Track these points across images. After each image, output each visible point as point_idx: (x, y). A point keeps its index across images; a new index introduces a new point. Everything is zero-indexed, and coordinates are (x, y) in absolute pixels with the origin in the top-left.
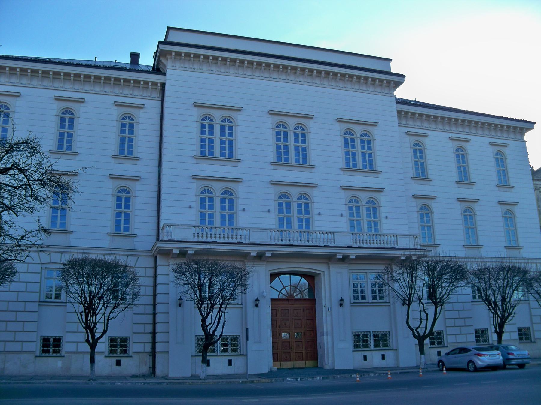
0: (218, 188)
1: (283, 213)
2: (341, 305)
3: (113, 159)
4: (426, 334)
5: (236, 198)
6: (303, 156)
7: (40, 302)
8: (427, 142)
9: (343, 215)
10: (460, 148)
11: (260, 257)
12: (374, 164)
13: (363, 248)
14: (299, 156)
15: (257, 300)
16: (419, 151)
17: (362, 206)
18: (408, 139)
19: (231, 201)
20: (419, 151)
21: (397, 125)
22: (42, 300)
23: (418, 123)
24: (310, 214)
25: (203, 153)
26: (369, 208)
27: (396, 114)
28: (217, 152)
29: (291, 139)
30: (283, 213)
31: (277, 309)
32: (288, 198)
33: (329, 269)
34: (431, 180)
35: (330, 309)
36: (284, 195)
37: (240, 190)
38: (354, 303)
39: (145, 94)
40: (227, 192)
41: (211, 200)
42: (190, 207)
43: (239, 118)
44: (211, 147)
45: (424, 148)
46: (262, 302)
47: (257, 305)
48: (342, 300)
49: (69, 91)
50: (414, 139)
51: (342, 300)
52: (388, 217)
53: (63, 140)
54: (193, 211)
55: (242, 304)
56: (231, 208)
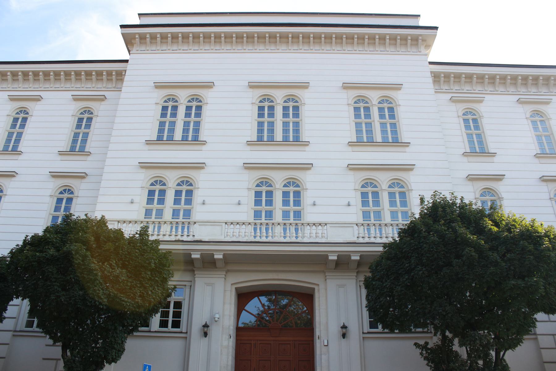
0: (278, 179)
2: (344, 336)
5: (409, 190)
7: (15, 331)
10: (537, 113)
12: (483, 139)
15: (206, 326)
16: (472, 122)
19: (297, 194)
20: (472, 122)
21: (433, 91)
22: (18, 329)
23: (467, 88)
25: (260, 139)
27: (430, 80)
28: (279, 135)
29: (278, 117)
32: (375, 186)
33: (326, 280)
35: (326, 344)
36: (264, 182)
37: (308, 179)
38: (368, 333)
41: (270, 194)
42: (349, 205)
43: (306, 97)
44: (271, 131)
45: (480, 117)
46: (214, 331)
47: (206, 334)
48: (344, 327)
50: (462, 107)
52: (206, 202)
54: (352, 209)
55: (187, 333)
56: (297, 203)
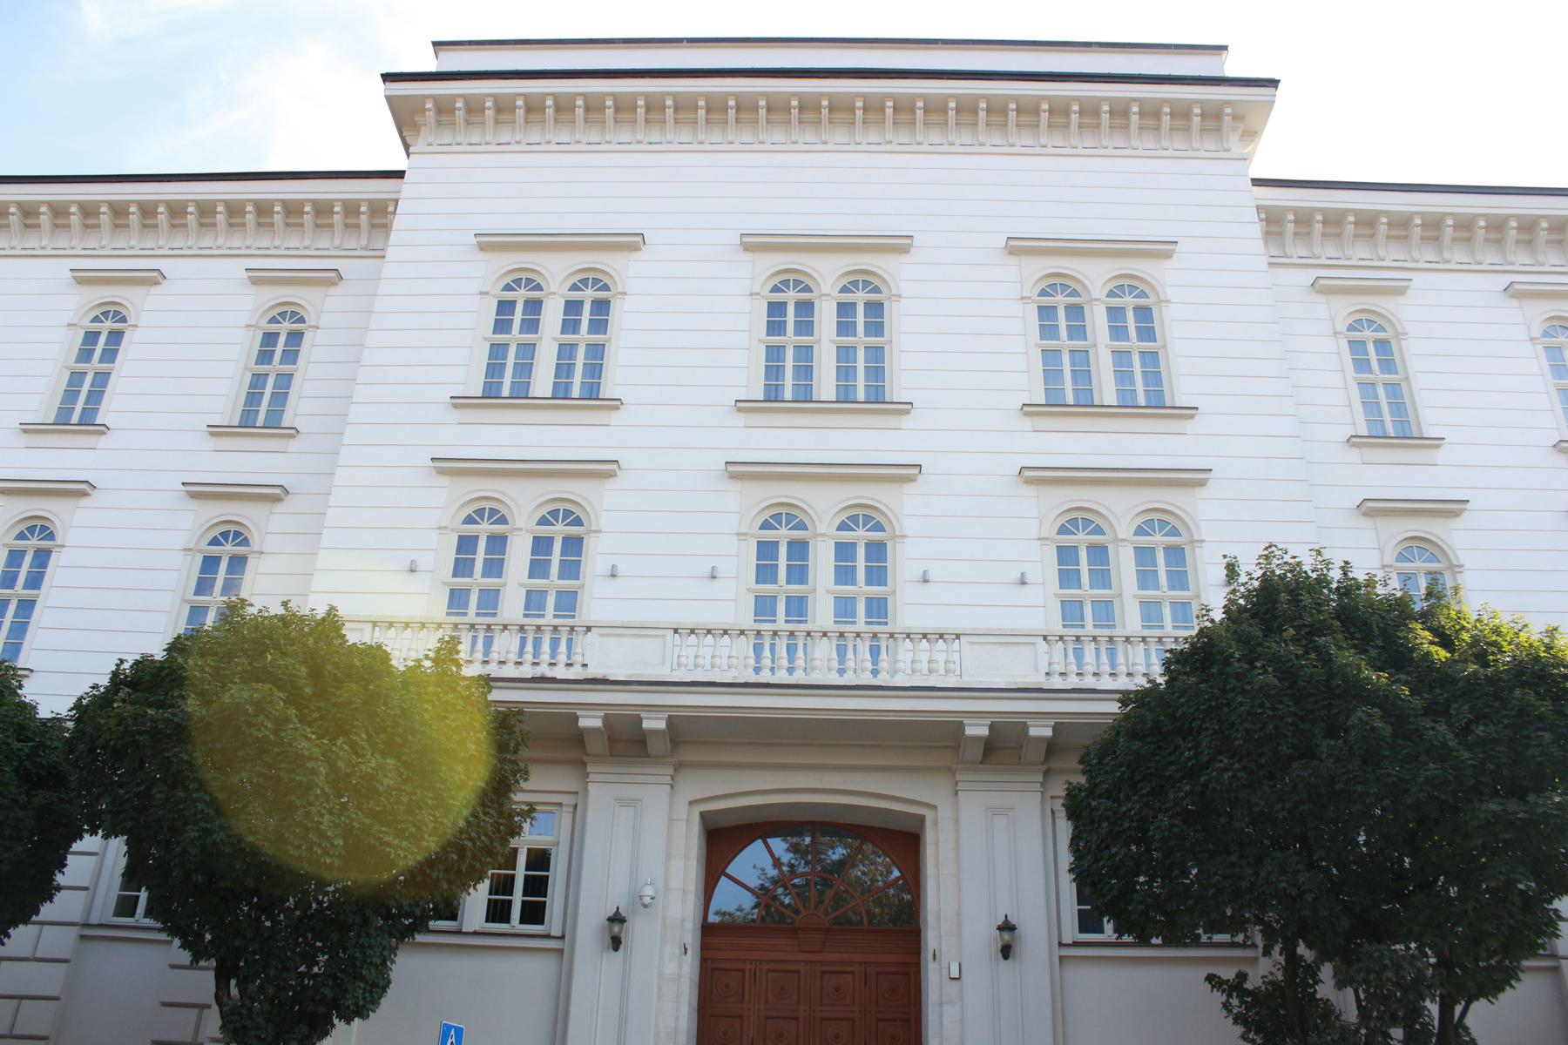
0: (824, 507)
1: (1157, 588)
3: (742, 416)
4: (159, 925)
6: (1146, 383)
8: (1402, 311)
9: (1029, 578)
11: (626, 743)
13: (553, 680)
14: (74, 401)
15: (617, 919)
17: (1117, 540)
18: (1321, 307)
19: (877, 551)
23: (1360, 252)
24: (1191, 586)
26: (549, 541)
27: (1256, 230)
28: (826, 385)
29: (824, 332)
30: (1157, 588)
31: (748, 966)
32: (1098, 530)
34: (1436, 443)
36: (784, 516)
37: (907, 509)
38: (1076, 944)
39: (352, 244)
40: (1155, 521)
45: (1397, 334)
46: (639, 933)
47: (616, 943)
48: (1007, 927)
49: (114, 252)
50: (1344, 308)
51: (1007, 927)
53: (570, 368)
54: (1032, 594)
55: (563, 937)
